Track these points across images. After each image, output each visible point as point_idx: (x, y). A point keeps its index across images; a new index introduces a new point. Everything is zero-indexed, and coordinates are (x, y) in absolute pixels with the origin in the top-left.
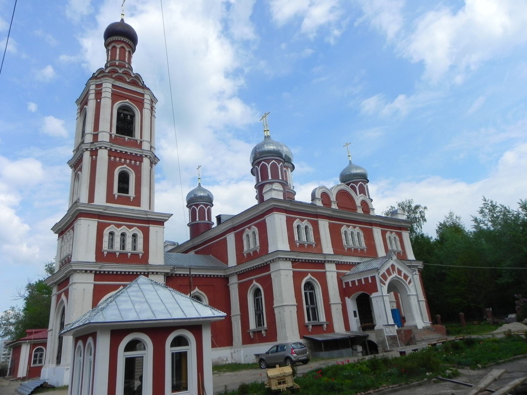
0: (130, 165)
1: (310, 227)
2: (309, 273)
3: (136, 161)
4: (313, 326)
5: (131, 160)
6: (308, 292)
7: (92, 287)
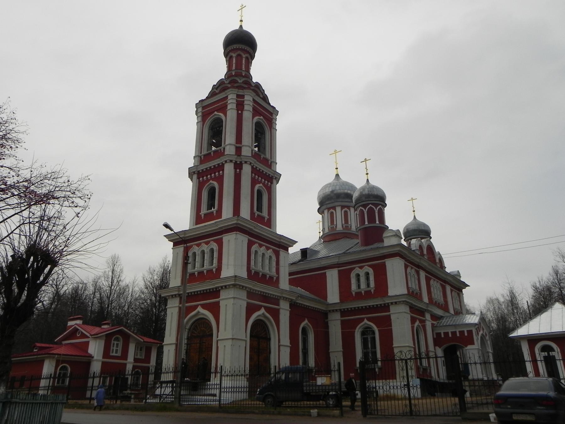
2: (263, 307)
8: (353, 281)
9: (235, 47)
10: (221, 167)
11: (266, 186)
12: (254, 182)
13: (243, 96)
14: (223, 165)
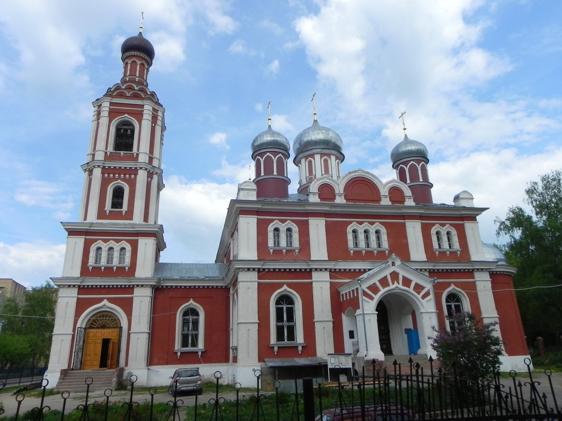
0: (124, 180)
1: (454, 232)
2: (285, 285)
3: (130, 175)
4: (278, 347)
5: (125, 174)
6: (453, 304)
7: (75, 300)
8: (92, 255)
9: (133, 54)
10: (135, 171)
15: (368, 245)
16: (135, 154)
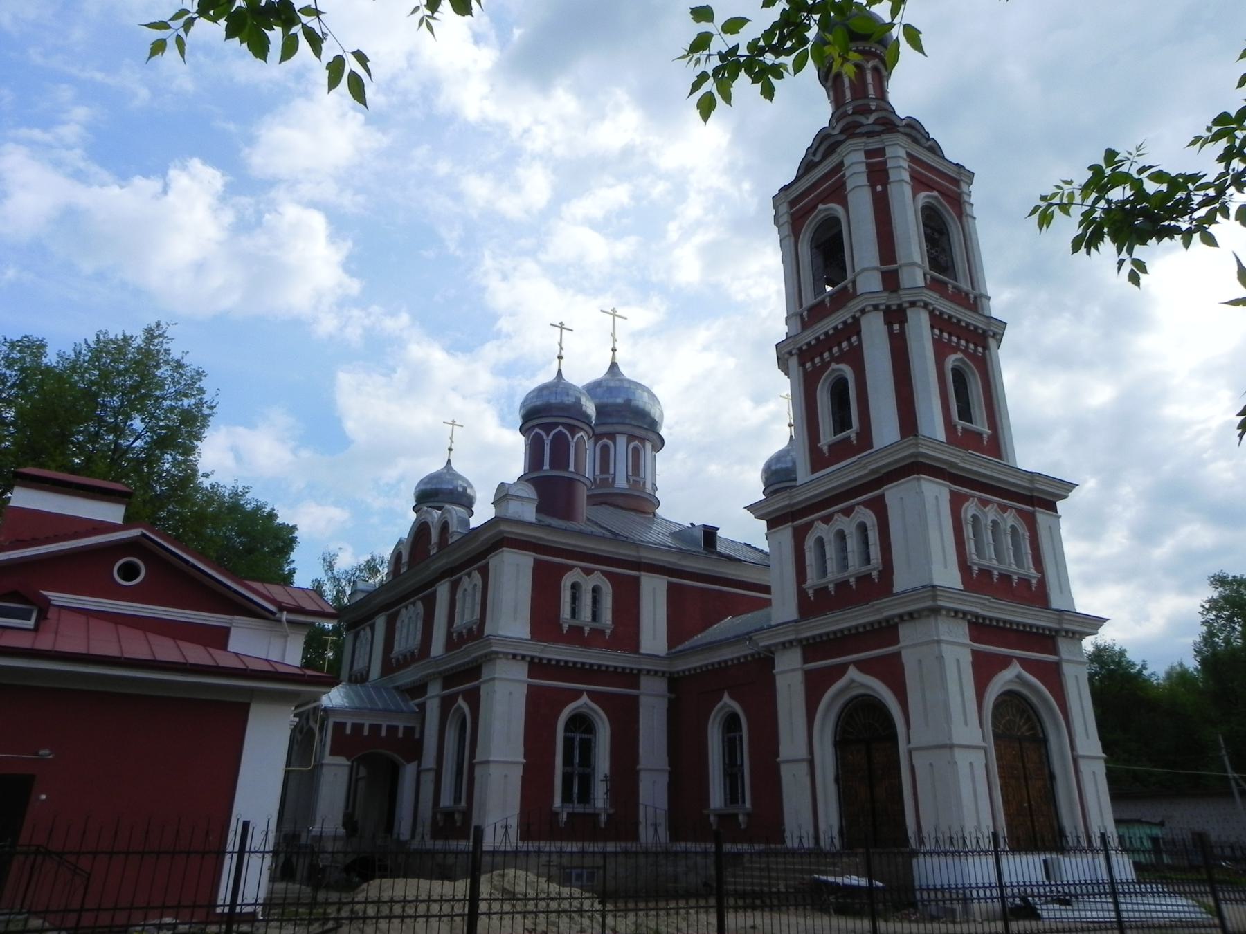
5: (830, 350)
7: (524, 690)
10: (853, 328)
11: (972, 356)
12: (941, 350)
13: (881, 152)
14: (856, 321)
15: (595, 617)
16: (850, 286)
